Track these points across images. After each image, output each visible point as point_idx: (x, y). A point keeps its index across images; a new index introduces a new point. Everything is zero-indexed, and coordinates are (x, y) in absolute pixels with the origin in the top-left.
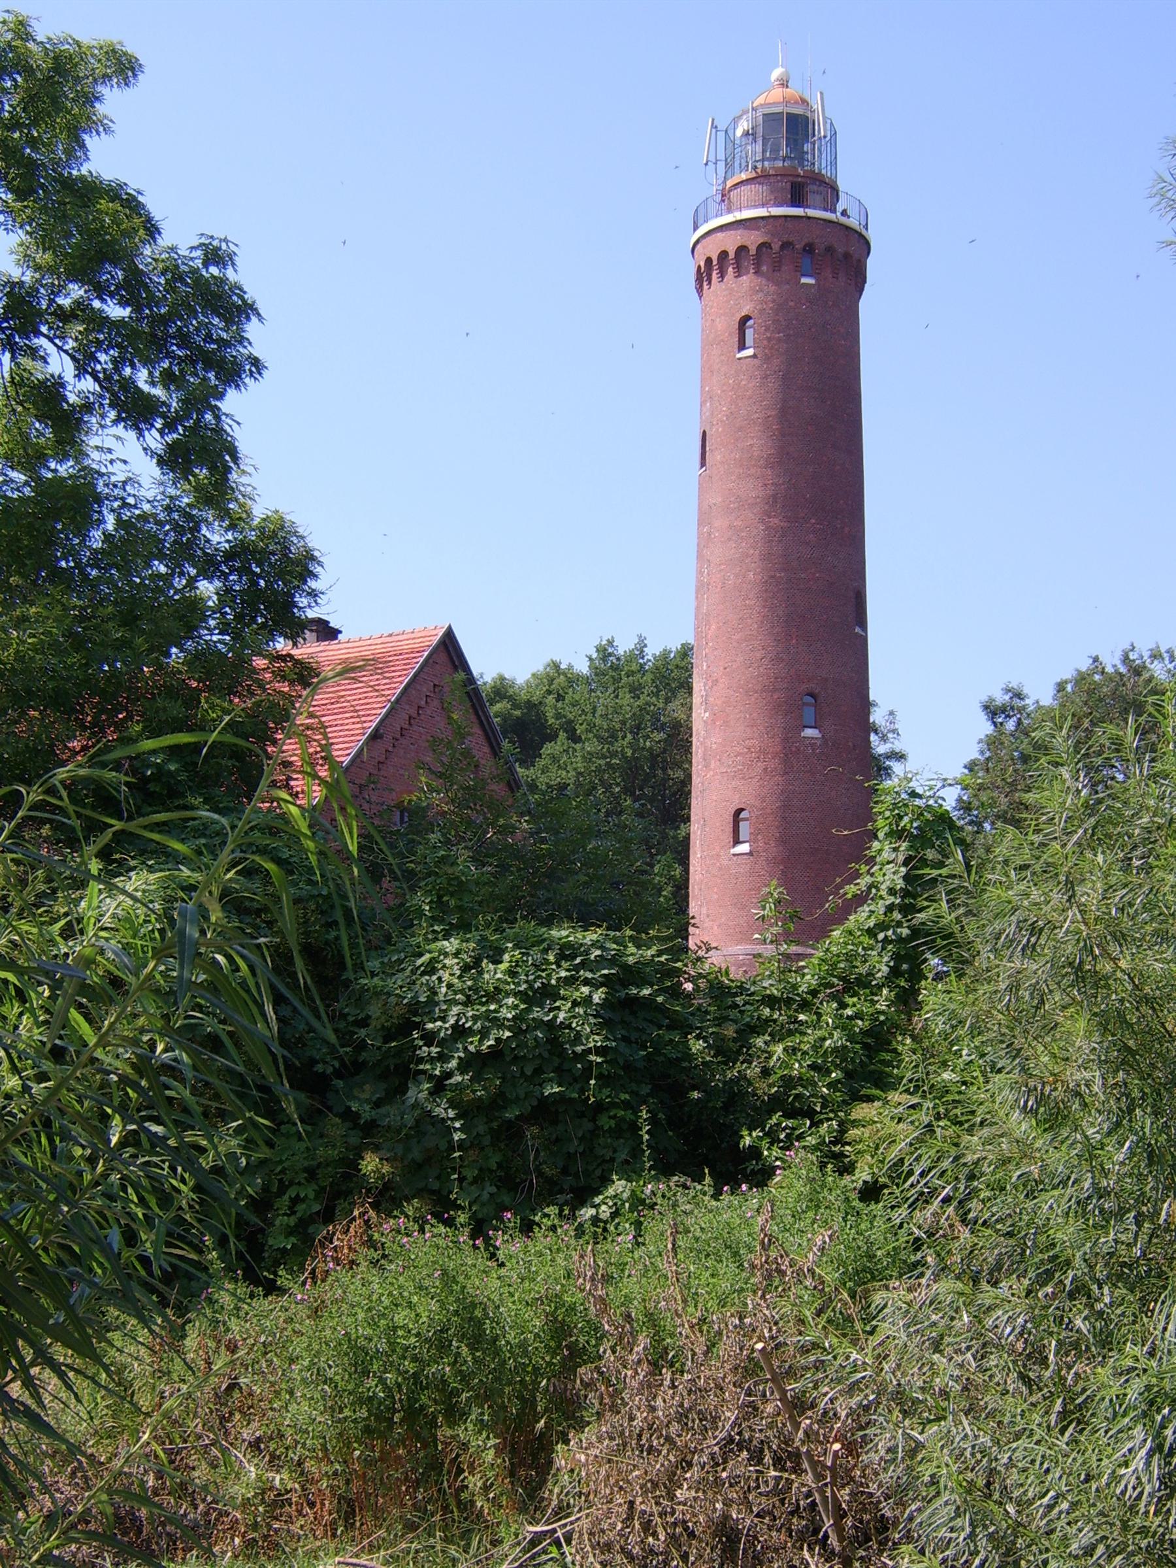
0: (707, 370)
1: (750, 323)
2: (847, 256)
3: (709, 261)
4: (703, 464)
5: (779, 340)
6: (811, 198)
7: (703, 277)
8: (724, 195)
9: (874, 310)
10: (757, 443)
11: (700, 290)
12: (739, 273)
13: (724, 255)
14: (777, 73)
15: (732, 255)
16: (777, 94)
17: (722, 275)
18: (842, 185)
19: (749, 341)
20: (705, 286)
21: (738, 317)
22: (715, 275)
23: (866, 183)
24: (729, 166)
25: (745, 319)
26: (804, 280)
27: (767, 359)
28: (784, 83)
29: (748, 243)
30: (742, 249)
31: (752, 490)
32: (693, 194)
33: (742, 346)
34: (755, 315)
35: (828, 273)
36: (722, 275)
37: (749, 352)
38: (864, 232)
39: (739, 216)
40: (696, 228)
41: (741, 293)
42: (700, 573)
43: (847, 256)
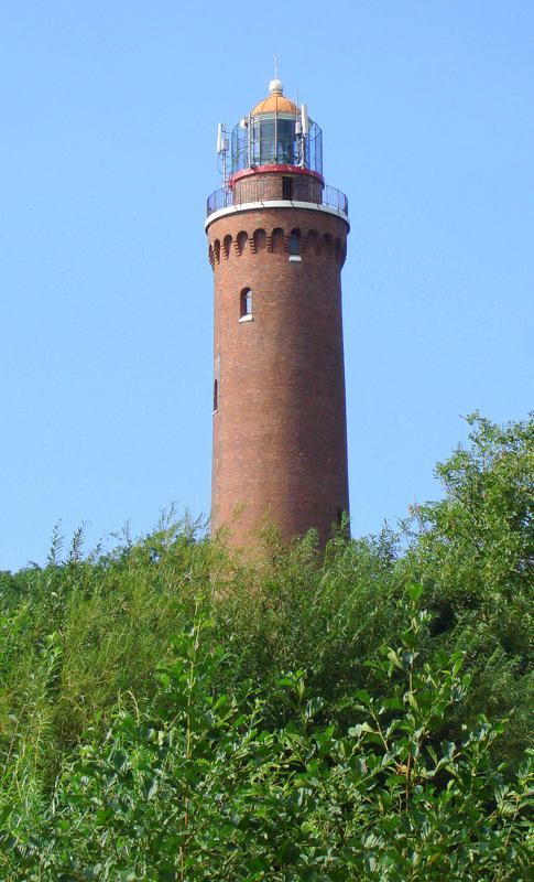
0: (219, 331)
1: (250, 294)
2: (327, 236)
3: (217, 242)
4: (215, 407)
5: (272, 308)
6: (295, 193)
7: (217, 250)
8: (232, 184)
9: (353, 277)
10: (257, 393)
11: (212, 261)
12: (255, 250)
13: (228, 239)
14: (273, 85)
15: (234, 238)
16: (271, 104)
17: (240, 248)
18: (329, 177)
19: (249, 309)
20: (216, 263)
21: (240, 288)
22: (222, 252)
23: (345, 182)
24: (235, 160)
25: (245, 291)
26: (292, 258)
27: (262, 323)
28: (280, 92)
29: (247, 230)
30: (259, 233)
31: (273, 423)
32: (202, 184)
33: (244, 312)
34: (252, 286)
35: (312, 251)
36: (240, 248)
37: (248, 317)
38: (343, 216)
39: (240, 207)
40: (210, 211)
41: (244, 267)
42: (214, 496)
43: (327, 236)
